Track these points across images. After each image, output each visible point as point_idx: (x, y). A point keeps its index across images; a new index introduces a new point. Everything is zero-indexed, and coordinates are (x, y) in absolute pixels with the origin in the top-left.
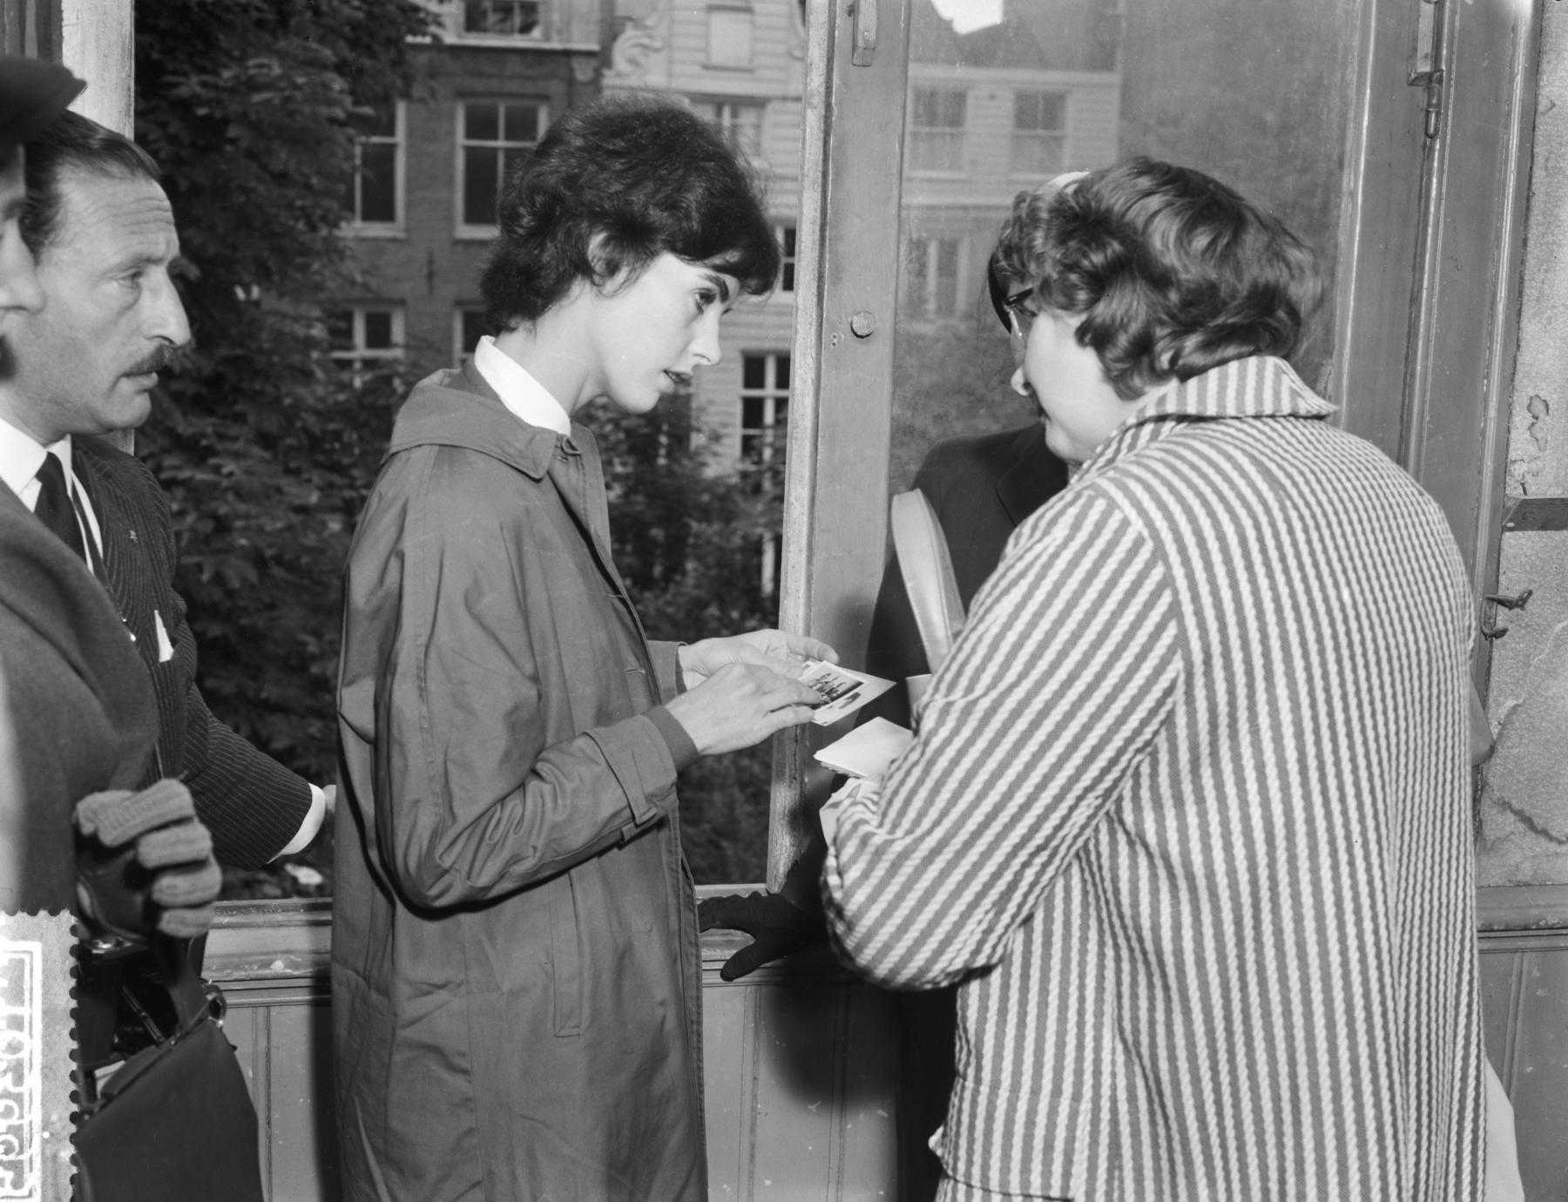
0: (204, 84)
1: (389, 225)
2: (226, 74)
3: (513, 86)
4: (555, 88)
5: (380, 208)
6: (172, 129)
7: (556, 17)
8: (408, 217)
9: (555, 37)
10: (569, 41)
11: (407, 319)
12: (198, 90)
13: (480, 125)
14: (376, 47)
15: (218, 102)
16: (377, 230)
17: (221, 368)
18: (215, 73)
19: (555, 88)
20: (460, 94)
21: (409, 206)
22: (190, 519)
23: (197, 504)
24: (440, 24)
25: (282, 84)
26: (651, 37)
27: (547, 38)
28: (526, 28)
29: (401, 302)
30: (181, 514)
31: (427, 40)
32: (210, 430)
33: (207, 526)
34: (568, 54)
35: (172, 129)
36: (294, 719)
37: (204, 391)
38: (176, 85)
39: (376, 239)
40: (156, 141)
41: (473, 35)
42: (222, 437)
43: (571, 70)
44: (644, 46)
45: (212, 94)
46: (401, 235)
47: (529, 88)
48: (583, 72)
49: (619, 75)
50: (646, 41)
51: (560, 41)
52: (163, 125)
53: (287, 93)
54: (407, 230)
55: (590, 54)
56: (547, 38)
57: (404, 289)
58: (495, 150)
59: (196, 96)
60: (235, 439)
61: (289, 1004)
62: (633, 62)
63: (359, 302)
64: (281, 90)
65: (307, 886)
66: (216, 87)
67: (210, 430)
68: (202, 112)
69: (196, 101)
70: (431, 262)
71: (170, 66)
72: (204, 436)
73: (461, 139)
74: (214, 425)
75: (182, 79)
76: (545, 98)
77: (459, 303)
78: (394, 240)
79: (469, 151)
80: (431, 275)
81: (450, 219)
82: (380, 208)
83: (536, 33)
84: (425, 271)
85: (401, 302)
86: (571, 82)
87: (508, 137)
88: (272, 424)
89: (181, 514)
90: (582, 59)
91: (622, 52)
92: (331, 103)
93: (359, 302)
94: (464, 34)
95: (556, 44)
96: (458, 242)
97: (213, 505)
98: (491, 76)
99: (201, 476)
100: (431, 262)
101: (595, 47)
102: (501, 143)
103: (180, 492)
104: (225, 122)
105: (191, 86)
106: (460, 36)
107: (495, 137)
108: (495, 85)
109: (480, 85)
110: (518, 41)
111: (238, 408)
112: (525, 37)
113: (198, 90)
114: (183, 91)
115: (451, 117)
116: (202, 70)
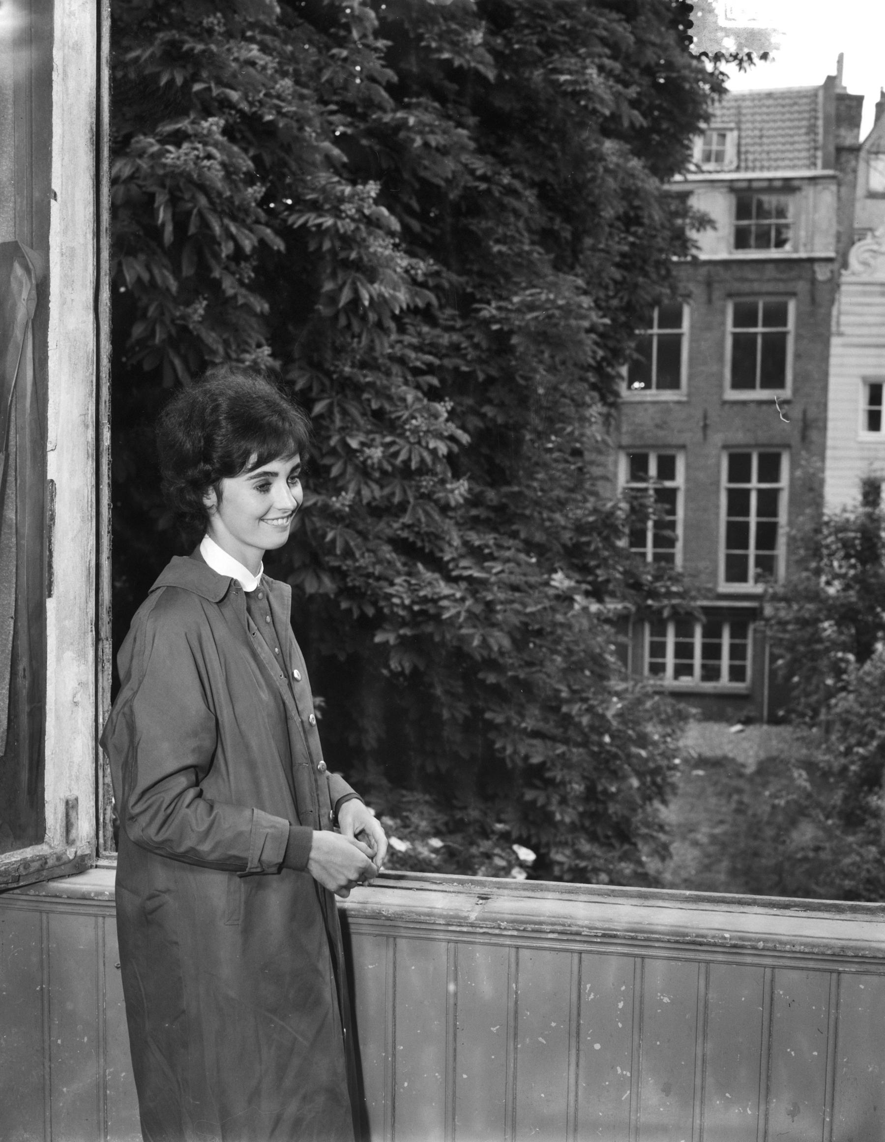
0: (499, 308)
1: (676, 392)
2: (516, 299)
3: (769, 287)
4: (802, 286)
5: (669, 378)
6: (476, 340)
7: (803, 233)
8: (689, 385)
9: (802, 248)
10: (812, 251)
11: (687, 459)
12: (494, 312)
13: (745, 316)
14: (647, 268)
15: (507, 319)
16: (668, 395)
17: (504, 500)
18: (508, 299)
19: (802, 286)
20: (730, 295)
21: (691, 377)
22: (469, 603)
23: (474, 593)
24: (698, 248)
25: (548, 306)
26: (878, 244)
27: (796, 250)
28: (780, 243)
29: (683, 447)
30: (463, 599)
31: (689, 258)
32: (491, 542)
33: (478, 609)
34: (811, 261)
35: (476, 340)
36: (549, 743)
37: (492, 515)
38: (479, 310)
39: (666, 402)
40: (466, 348)
41: (740, 251)
42: (500, 547)
43: (814, 272)
44: (874, 251)
45: (503, 315)
46: (684, 399)
47: (781, 287)
48: (822, 273)
49: (853, 274)
50: (875, 247)
51: (806, 251)
52: (470, 337)
53: (550, 312)
54: (689, 395)
55: (829, 260)
56: (796, 250)
57: (686, 438)
58: (756, 334)
59: (493, 317)
60: (509, 548)
61: (611, 953)
62: (865, 264)
63: (654, 447)
64: (547, 309)
65: (525, 861)
66: (507, 309)
67: (491, 542)
68: (495, 327)
69: (493, 320)
70: (705, 417)
71: (478, 296)
72: (487, 546)
73: (730, 328)
74: (495, 539)
75: (484, 306)
76: (793, 294)
77: (725, 447)
78: (679, 403)
79: (736, 336)
80: (705, 427)
81: (721, 386)
82: (669, 378)
83: (788, 247)
84: (701, 424)
85: (683, 447)
86: (813, 281)
87: (765, 325)
88: (539, 537)
89: (463, 599)
90: (823, 264)
91: (856, 255)
92: (584, 317)
93: (654, 447)
94: (734, 251)
95: (803, 255)
96: (725, 403)
97: (484, 593)
98: (752, 281)
99: (476, 574)
100: (705, 417)
101: (832, 254)
102: (760, 329)
103: (463, 585)
104: (511, 332)
105: (489, 311)
106: (730, 253)
107: (755, 325)
108: (756, 286)
109: (745, 287)
110: (774, 253)
111: (514, 527)
112: (780, 250)
113: (494, 312)
114: (485, 314)
115: (723, 312)
116: (500, 298)
